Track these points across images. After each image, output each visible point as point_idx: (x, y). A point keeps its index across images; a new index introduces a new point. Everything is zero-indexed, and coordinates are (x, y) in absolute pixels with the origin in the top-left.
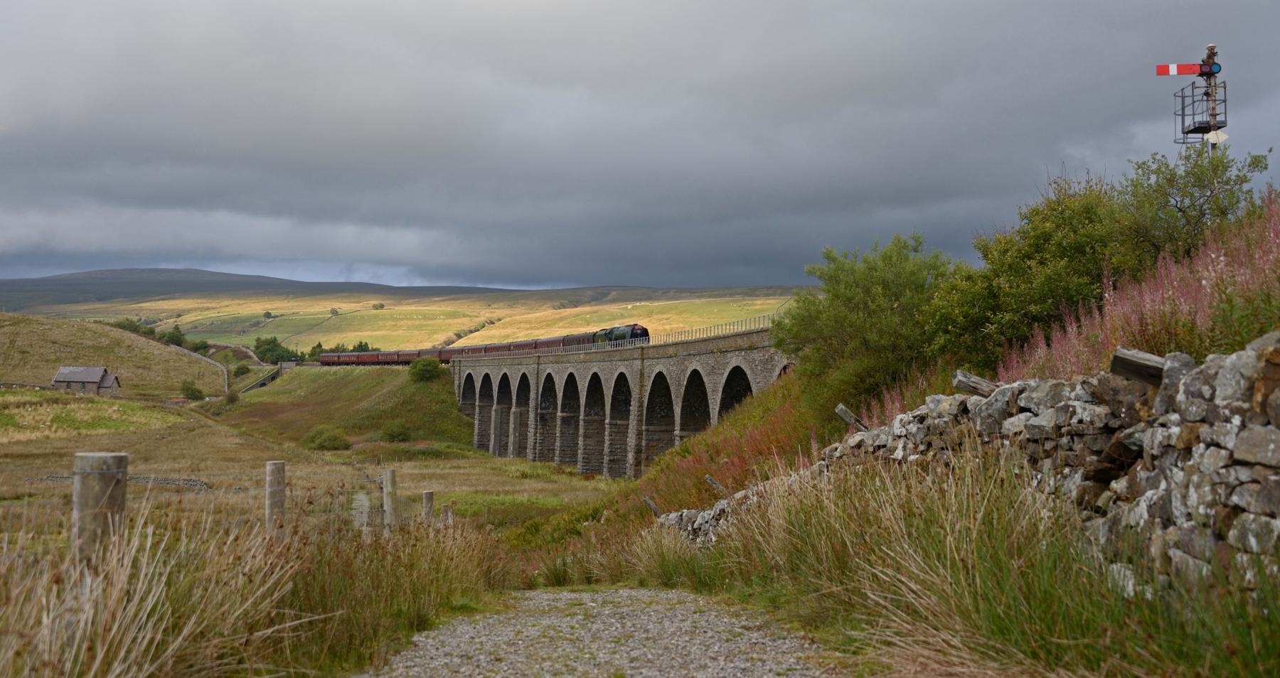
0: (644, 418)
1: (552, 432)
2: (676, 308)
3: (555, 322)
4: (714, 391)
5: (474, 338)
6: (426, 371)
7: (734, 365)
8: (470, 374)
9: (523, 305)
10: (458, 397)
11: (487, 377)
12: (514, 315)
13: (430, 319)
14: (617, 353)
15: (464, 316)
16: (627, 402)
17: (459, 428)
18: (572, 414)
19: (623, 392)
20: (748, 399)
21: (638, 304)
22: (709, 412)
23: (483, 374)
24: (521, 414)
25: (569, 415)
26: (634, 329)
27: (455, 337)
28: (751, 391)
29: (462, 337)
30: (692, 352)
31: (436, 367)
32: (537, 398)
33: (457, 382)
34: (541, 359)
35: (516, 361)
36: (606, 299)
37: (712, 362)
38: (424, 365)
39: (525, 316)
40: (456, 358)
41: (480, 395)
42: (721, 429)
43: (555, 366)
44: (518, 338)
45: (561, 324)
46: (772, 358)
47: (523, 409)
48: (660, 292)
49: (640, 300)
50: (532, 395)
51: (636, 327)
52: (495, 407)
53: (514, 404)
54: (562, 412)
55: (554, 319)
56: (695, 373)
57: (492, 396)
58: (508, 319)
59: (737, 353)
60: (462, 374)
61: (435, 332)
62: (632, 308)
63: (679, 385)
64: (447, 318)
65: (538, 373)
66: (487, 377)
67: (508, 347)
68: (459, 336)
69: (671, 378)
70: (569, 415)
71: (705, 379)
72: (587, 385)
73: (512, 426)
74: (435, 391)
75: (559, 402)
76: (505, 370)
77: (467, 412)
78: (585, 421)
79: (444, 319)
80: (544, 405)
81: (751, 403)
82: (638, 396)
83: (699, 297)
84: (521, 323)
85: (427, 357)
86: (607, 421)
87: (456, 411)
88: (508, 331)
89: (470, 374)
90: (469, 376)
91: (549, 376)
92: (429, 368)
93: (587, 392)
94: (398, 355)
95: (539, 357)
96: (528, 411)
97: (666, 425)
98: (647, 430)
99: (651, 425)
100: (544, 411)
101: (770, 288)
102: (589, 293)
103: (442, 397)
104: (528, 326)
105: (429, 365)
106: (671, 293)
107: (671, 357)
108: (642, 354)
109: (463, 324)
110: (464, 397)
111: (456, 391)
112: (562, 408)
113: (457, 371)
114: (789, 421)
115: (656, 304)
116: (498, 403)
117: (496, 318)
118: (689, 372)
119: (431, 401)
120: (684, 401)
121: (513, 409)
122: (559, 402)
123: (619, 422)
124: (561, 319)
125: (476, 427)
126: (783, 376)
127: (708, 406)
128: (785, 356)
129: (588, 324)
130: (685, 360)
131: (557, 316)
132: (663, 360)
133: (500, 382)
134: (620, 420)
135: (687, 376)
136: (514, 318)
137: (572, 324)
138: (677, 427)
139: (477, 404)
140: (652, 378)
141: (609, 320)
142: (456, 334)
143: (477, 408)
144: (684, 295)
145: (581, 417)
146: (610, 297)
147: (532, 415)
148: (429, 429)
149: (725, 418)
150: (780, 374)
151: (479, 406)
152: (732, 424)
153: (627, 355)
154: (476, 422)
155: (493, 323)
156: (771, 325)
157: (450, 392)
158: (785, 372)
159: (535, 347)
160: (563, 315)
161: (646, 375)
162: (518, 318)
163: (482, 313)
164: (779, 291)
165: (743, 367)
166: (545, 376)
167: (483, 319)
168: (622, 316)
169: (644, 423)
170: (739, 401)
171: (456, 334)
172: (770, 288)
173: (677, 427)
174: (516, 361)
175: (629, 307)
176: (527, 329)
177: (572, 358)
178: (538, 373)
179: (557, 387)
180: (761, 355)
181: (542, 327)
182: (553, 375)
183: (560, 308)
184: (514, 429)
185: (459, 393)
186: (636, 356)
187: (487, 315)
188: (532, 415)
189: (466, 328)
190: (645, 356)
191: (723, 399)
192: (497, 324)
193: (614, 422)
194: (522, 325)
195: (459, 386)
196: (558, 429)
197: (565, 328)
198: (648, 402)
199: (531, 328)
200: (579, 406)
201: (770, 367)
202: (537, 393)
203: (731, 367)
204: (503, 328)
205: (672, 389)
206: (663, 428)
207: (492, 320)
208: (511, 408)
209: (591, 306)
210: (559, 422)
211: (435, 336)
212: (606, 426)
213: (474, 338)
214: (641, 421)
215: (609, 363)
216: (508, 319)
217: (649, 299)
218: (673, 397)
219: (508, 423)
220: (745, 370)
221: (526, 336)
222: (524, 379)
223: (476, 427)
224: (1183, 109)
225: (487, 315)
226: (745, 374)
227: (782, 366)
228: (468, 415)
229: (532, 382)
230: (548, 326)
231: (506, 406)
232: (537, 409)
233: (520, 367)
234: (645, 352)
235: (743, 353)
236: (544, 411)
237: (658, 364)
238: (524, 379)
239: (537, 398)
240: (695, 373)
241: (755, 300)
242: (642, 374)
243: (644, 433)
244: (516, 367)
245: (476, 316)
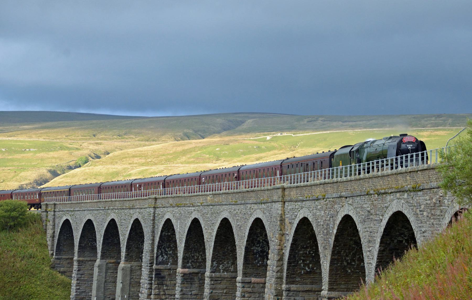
0: (285, 274)
1: (170, 292)
2: (325, 140)
3: (176, 155)
4: (369, 241)
5: (74, 176)
6: (9, 217)
7: (395, 210)
8: (67, 222)
9: (137, 134)
10: (51, 250)
11: (89, 224)
12: (126, 147)
13: (16, 152)
14: (253, 194)
15: (62, 148)
16: (264, 255)
17: (50, 290)
18: (196, 270)
19: (259, 242)
20: (412, 252)
21: (279, 135)
22: (364, 267)
23: (85, 221)
24: (131, 271)
25: (192, 270)
26: (401, 142)
27: (49, 175)
28: (415, 242)
29: (58, 175)
30: (343, 194)
31: (23, 213)
32: (153, 251)
33: (50, 232)
34: (158, 201)
35: (127, 204)
36: (240, 128)
37: (367, 206)
38: (7, 211)
39: (140, 149)
40: (46, 200)
41: (80, 246)
42: (378, 289)
43: (176, 210)
44: (130, 175)
45: (184, 159)
46: (440, 202)
47: (134, 264)
48: (306, 120)
49: (282, 130)
50: (147, 246)
51: (406, 139)
52: (98, 262)
53: (123, 258)
54: (184, 267)
55: (175, 153)
56: (347, 219)
57: (95, 248)
58: (117, 153)
59: (398, 195)
60: (57, 221)
61: (23, 169)
62: (271, 140)
63: (328, 233)
64: (40, 152)
65: (154, 220)
66: (89, 224)
67: (131, 186)
68: (55, 174)
69: (318, 225)
70: (192, 270)
71: (359, 227)
72: (215, 233)
73: (119, 285)
74: (20, 243)
75: (180, 255)
76: (113, 216)
77: (62, 269)
78: (211, 278)
79: (35, 152)
80: (160, 258)
81: (416, 258)
82: (277, 247)
83: (353, 127)
84: (134, 157)
85: (15, 200)
86: (239, 278)
87: (48, 268)
88: (118, 167)
89: (67, 222)
90: (67, 223)
91: (168, 222)
92: (14, 214)
93: (215, 242)
94: (40, 194)
95: (156, 199)
96: (141, 266)
97: (312, 283)
98: (288, 290)
99: (293, 283)
100: (160, 267)
101: (439, 116)
102: (219, 120)
103: (30, 251)
104: (143, 161)
105: (14, 210)
106: (319, 122)
107: (318, 199)
108: (283, 196)
109: (61, 159)
110: (59, 250)
111: (49, 243)
112: (183, 262)
113: (50, 217)
114: (462, 280)
115: (301, 135)
116: (103, 257)
117: (103, 151)
118: (339, 218)
119: (14, 256)
120: (333, 253)
121: (122, 265)
122: (180, 255)
123: (253, 280)
124: (184, 153)
125: (74, 288)
126: (454, 224)
127: (362, 260)
128: (456, 199)
129: (217, 160)
130: (335, 203)
131: (180, 149)
132: (308, 203)
133: (106, 231)
134: (255, 277)
135: (338, 222)
136: (125, 151)
137: (198, 159)
138: (325, 286)
139: (76, 258)
140: (295, 225)
141: (244, 154)
142: (50, 171)
143: (75, 263)
144: (335, 124)
145: (207, 274)
146: (244, 126)
147: (145, 272)
148: (11, 292)
149: (383, 276)
150: (451, 222)
151: (79, 261)
152: (391, 284)
153: (263, 198)
154: (74, 282)
155: (98, 157)
156: (439, 160)
157: (41, 244)
158: (456, 220)
159: (238, 178)
160: (186, 147)
161: (287, 221)
162: (130, 151)
163: (85, 144)
164: (450, 121)
165: (405, 212)
166: (163, 223)
167: (86, 152)
168: (260, 150)
169: (284, 281)
170: (400, 255)
171: (50, 171)
172: (439, 116)
173: (325, 286)
174: (127, 204)
175: (268, 138)
176: (142, 165)
177: (198, 201)
178: (154, 220)
179: (177, 236)
180: (427, 198)
181: (161, 163)
182: (173, 221)
183: (182, 139)
184: (123, 290)
185: (53, 245)
186: (275, 198)
187: (91, 147)
188: (145, 272)
189: (64, 164)
190: (287, 198)
191: (381, 252)
192: (104, 158)
193: (247, 279)
194: (136, 160)
195: (53, 237)
196: (178, 289)
197: (189, 163)
198: (290, 255)
199: (147, 164)
200: (204, 260)
201: (438, 213)
202: (153, 244)
203: (391, 213)
204: (111, 163)
205: (319, 238)
206: (308, 287)
207: (98, 153)
208: (119, 263)
209: (221, 137)
210: (179, 280)
211: (23, 174)
212: (238, 285)
213: (74, 176)
214: (281, 278)
215: (242, 207)
216: (117, 153)
217: (292, 128)
218: (320, 249)
219: (115, 282)
220: (408, 216)
221: (140, 173)
222: (137, 225)
223: (74, 288)
224: (54, 219)
225: (91, 147)
226: (408, 221)
227: (453, 212)
228: (63, 273)
229: (147, 230)
230: (168, 161)
231: (113, 261)
232: (152, 263)
233: (131, 211)
234: (286, 193)
235: (406, 196)
236: (160, 267)
237: (302, 208)
238: (137, 225)
239: (153, 251)
240: (347, 219)
241: (421, 131)
242: (282, 221)
243: (284, 293)
244: (126, 211)
245: (77, 149)
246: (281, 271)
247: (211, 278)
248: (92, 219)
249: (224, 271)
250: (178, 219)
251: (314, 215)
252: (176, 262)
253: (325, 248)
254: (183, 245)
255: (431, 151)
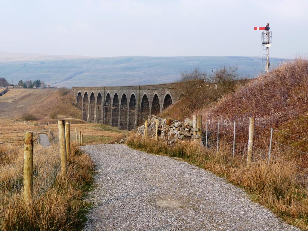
16: (135, 104)
18: (117, 108)
19: (133, 101)
43: (110, 90)
50: (102, 101)
54: (113, 107)
60: (77, 92)
70: (115, 108)
72: (121, 98)
75: (112, 104)
86: (128, 110)
93: (122, 100)
97: (148, 112)
135: (153, 96)
178: (104, 93)
182: (110, 94)
210: (112, 110)
214: (139, 111)
232: (104, 106)
239: (104, 102)
246: (139, 109)
247: (120, 110)
248: (87, 92)
249: (124, 108)
250: (111, 93)
251: (148, 94)
252: (111, 105)
253: (150, 103)
254: (113, 101)
255: (267, 28)
